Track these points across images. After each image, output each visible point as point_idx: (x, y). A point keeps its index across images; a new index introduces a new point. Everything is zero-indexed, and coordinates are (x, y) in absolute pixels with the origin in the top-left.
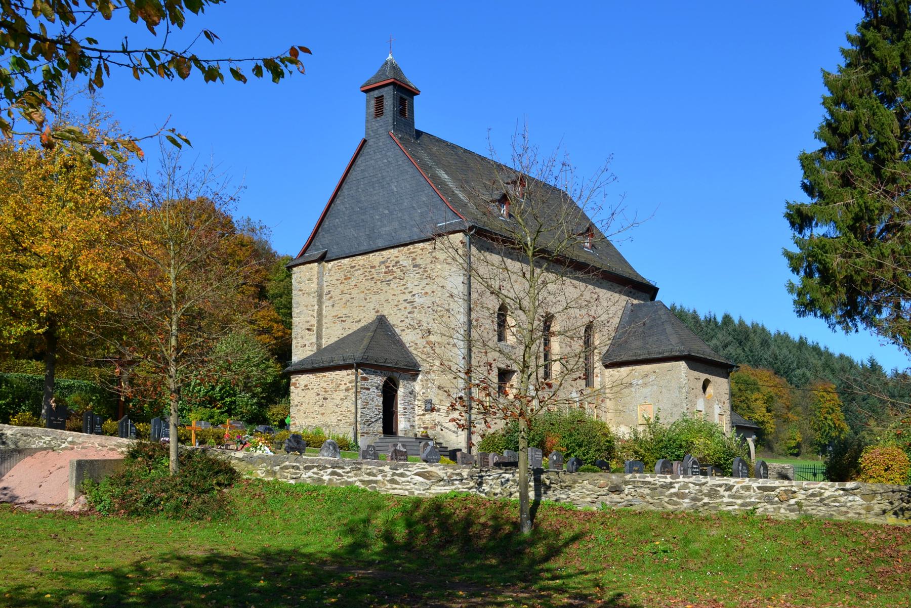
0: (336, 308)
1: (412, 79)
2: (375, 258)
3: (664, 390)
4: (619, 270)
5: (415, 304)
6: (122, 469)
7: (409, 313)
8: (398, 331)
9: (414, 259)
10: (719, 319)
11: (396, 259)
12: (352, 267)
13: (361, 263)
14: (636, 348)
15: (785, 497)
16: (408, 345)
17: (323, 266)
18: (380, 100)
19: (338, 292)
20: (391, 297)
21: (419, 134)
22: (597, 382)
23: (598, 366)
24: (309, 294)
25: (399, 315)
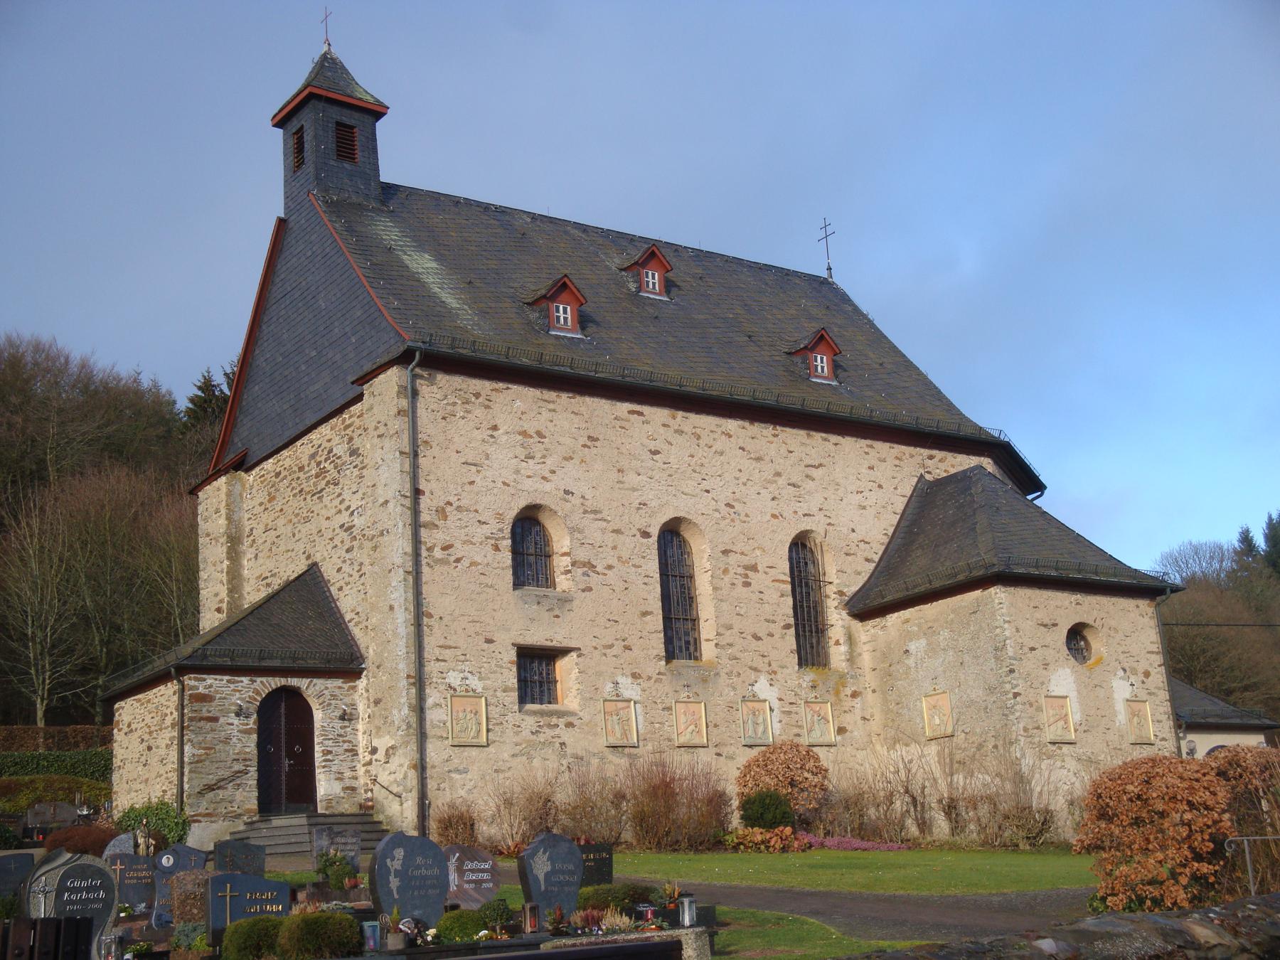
0: (260, 561)
1: (370, 80)
2: (302, 449)
3: (967, 658)
4: (948, 426)
5: (355, 531)
6: (566, 919)
7: (348, 551)
8: (333, 590)
9: (351, 439)
10: (191, 406)
11: (328, 445)
12: (278, 475)
13: (288, 463)
14: (917, 574)
15: (763, 847)
16: (347, 618)
17: (241, 479)
18: (299, 135)
19: (261, 528)
20: (325, 524)
21: (390, 190)
22: (837, 655)
23: (837, 619)
24: (216, 540)
25: (335, 559)
